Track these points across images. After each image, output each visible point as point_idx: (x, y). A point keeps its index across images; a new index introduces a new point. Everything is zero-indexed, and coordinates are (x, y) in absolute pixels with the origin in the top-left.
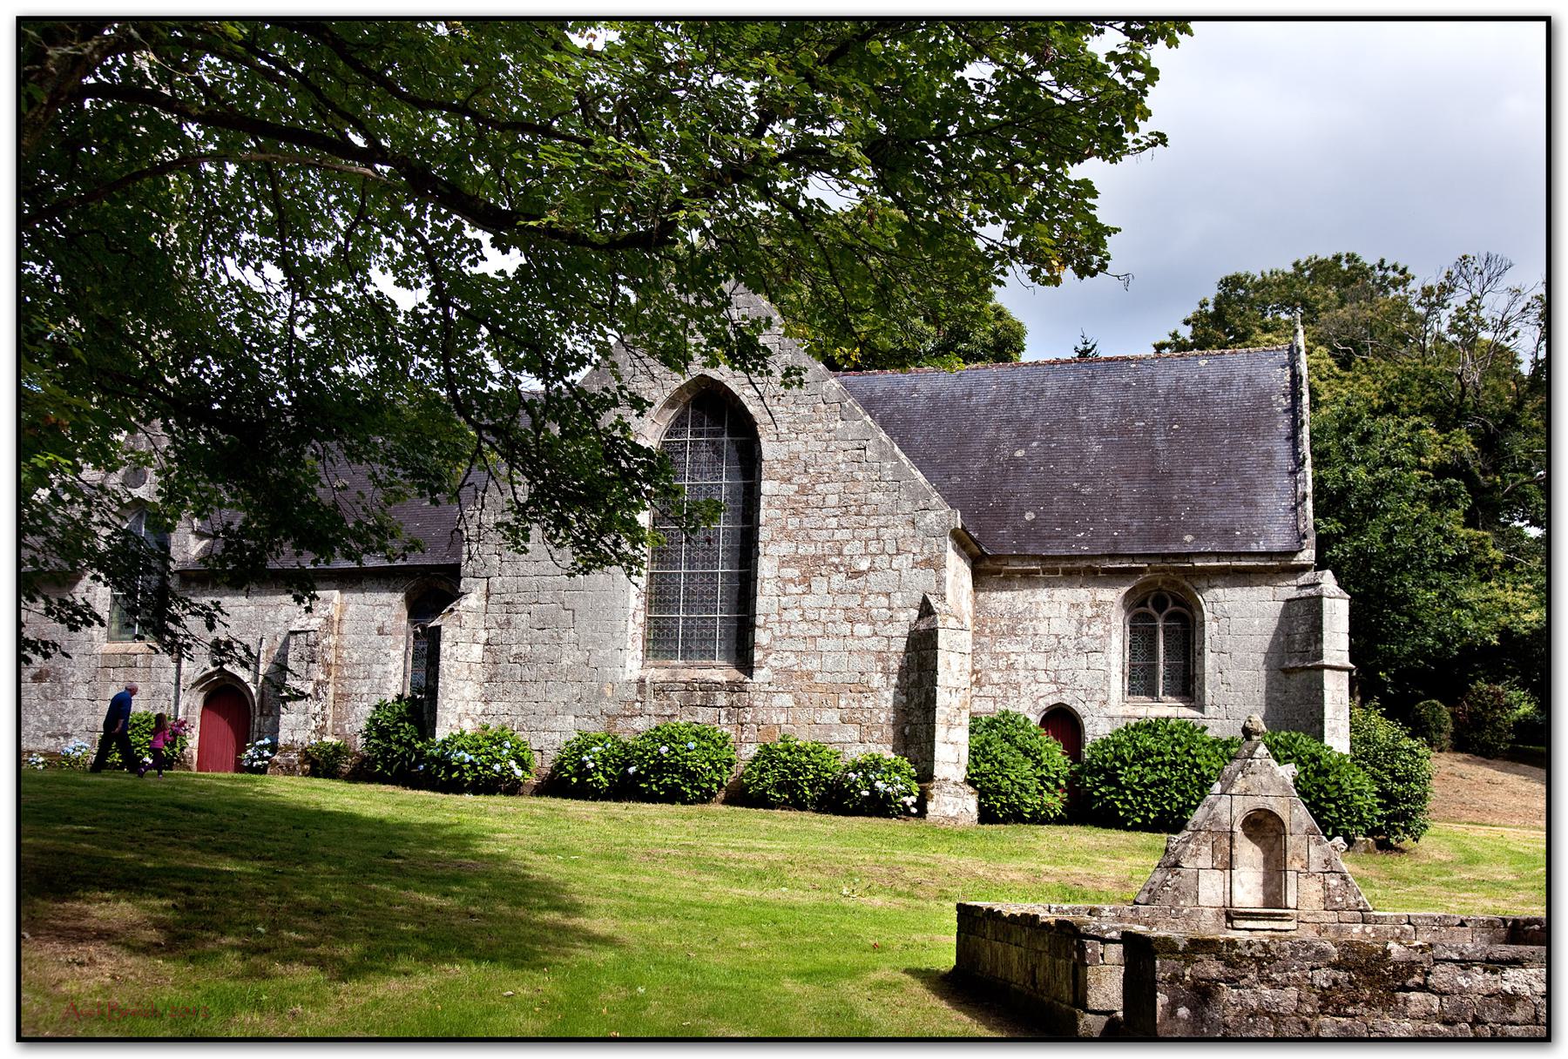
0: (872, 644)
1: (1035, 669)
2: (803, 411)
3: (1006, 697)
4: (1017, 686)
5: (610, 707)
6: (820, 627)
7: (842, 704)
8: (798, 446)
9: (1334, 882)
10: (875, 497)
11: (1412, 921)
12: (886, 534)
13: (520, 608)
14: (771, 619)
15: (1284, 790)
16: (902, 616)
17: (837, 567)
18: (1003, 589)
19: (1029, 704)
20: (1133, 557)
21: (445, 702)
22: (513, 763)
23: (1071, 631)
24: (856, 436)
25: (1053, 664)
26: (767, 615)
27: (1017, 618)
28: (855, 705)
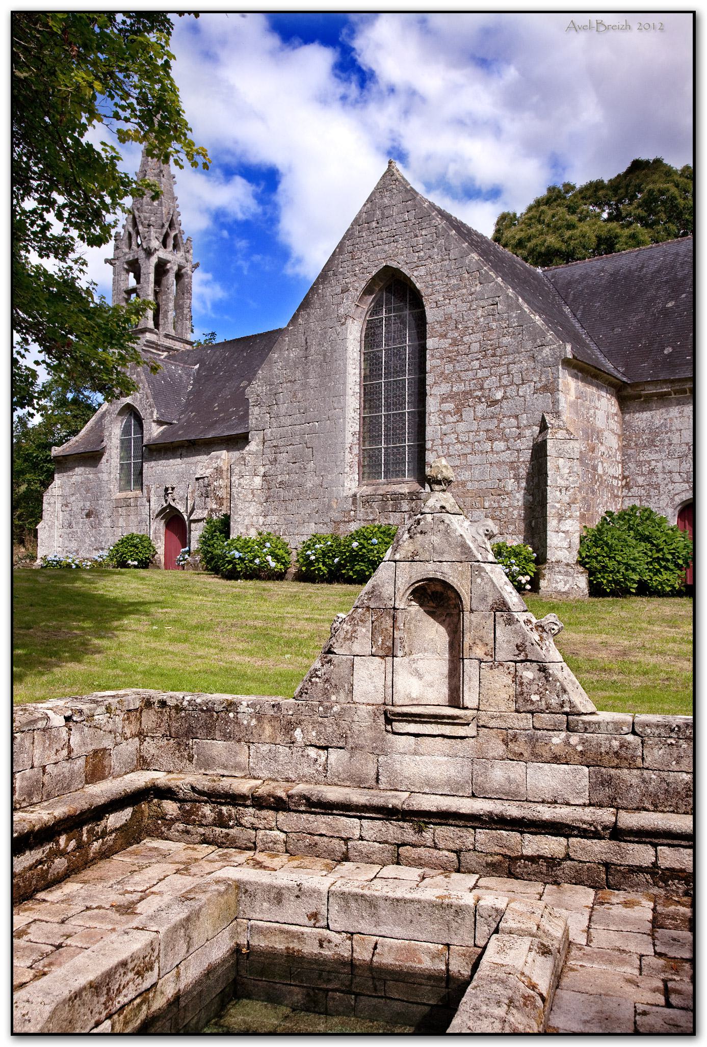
0: (507, 456)
1: (670, 472)
2: (454, 281)
3: (649, 496)
4: (657, 487)
5: (335, 515)
6: (470, 446)
7: (487, 505)
8: (451, 309)
9: (529, 674)
10: (506, 340)
11: (638, 729)
12: (514, 368)
13: (282, 449)
14: (436, 443)
15: (463, 553)
16: (527, 432)
17: (480, 399)
18: (643, 410)
19: (667, 500)
21: (236, 517)
22: (269, 558)
24: (490, 295)
26: (433, 440)
27: (655, 433)
28: (496, 505)
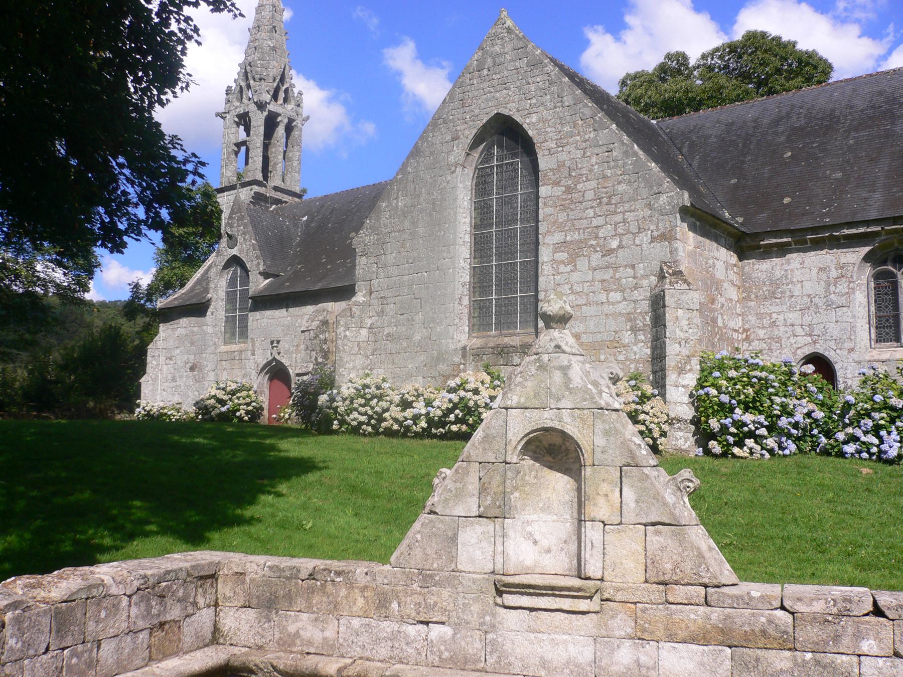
0: (623, 307)
1: (793, 325)
2: (567, 129)
4: (779, 340)
8: (563, 156)
16: (645, 283)
20: (868, 223)
21: (341, 370)
23: (820, 289)
25: (807, 319)
26: (546, 291)
